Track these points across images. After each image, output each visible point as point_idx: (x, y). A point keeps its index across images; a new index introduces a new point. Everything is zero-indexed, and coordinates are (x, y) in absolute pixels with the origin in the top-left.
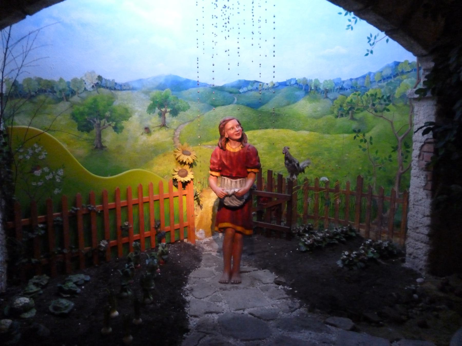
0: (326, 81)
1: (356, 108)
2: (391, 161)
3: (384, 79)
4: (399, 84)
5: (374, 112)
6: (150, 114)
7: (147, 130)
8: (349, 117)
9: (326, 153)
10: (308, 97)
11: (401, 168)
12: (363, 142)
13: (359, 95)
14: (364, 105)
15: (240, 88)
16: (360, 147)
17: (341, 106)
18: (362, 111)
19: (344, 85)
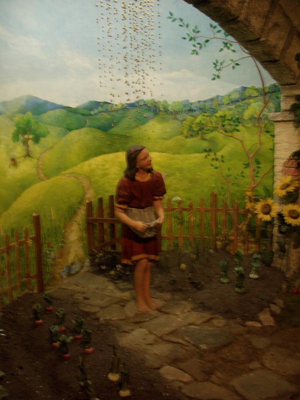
0: (174, 102)
1: (205, 129)
2: (243, 176)
3: (232, 102)
4: (247, 107)
5: (223, 132)
6: (14, 142)
7: (14, 162)
8: (199, 137)
9: (177, 172)
10: (156, 118)
11: (253, 182)
12: (215, 161)
13: (208, 116)
14: (214, 126)
15: (91, 109)
16: (212, 165)
17: (191, 127)
18: (212, 131)
19: (192, 107)
